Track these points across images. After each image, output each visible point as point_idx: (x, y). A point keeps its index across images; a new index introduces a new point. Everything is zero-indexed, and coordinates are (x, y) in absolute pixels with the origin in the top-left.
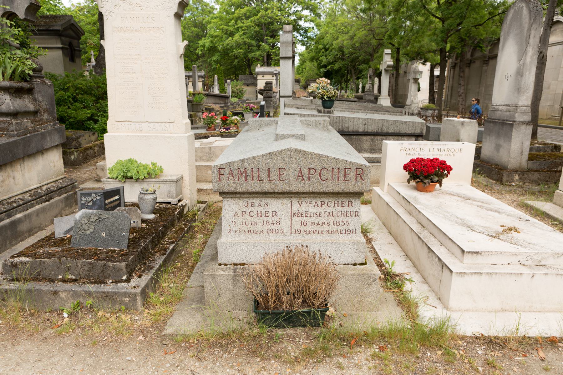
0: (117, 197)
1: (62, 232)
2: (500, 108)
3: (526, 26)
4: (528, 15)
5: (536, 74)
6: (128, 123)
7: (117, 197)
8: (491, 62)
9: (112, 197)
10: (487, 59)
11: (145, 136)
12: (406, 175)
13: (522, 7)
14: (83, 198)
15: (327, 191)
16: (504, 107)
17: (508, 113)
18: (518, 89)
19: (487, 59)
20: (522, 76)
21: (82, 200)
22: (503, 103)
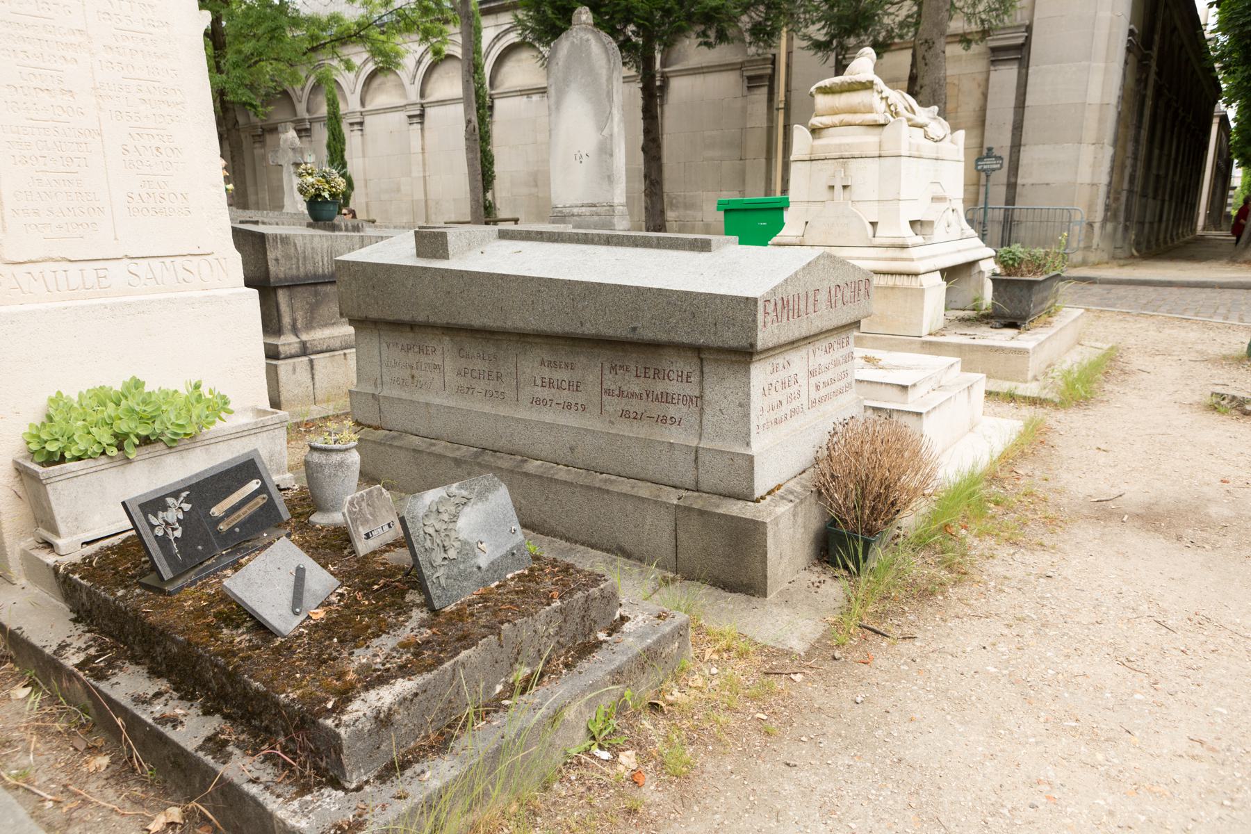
0: (254, 485)
1: (286, 611)
2: (575, 210)
3: (604, 73)
4: (603, 56)
5: (468, 159)
6: (54, 266)
7: (254, 485)
8: (269, 138)
9: (230, 491)
10: (259, 131)
11: (129, 305)
12: (53, 395)
13: (588, 40)
14: (154, 521)
15: (839, 324)
16: (584, 209)
17: (596, 218)
18: (609, 177)
19: (259, 131)
20: (611, 155)
21: (153, 527)
22: (579, 203)
